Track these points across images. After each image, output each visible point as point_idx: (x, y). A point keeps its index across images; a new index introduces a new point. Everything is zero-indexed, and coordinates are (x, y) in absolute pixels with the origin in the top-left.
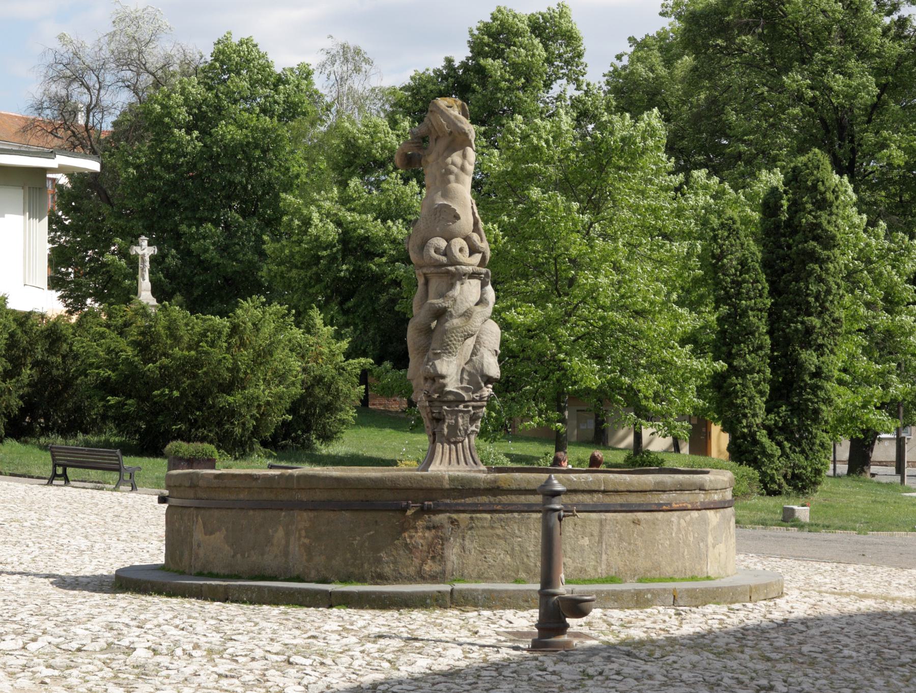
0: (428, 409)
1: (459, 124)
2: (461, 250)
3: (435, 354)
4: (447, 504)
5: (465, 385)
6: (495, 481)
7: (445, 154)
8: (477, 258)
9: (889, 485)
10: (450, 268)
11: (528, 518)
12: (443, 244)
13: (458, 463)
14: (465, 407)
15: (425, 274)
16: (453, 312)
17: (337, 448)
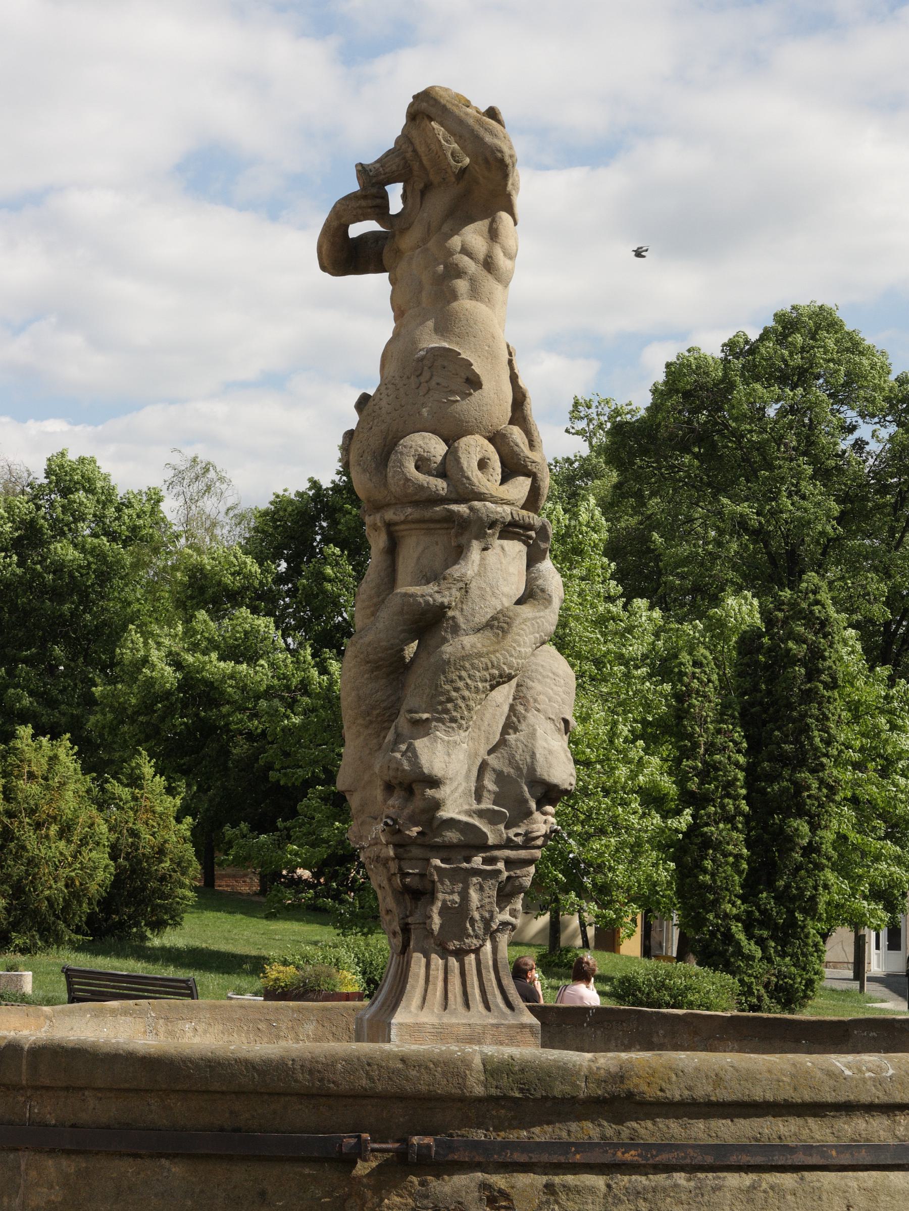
0: (393, 867)
1: (488, 139)
2: (483, 464)
3: (416, 723)
4: (476, 1145)
5: (486, 805)
6: (620, 1077)
7: (446, 228)
8: (520, 488)
9: (846, 993)
10: (455, 507)
11: (716, 1189)
12: (437, 448)
13: (467, 1005)
14: (486, 861)
15: (389, 525)
16: (461, 620)
17: (171, 938)
